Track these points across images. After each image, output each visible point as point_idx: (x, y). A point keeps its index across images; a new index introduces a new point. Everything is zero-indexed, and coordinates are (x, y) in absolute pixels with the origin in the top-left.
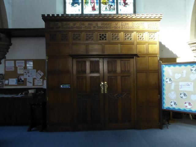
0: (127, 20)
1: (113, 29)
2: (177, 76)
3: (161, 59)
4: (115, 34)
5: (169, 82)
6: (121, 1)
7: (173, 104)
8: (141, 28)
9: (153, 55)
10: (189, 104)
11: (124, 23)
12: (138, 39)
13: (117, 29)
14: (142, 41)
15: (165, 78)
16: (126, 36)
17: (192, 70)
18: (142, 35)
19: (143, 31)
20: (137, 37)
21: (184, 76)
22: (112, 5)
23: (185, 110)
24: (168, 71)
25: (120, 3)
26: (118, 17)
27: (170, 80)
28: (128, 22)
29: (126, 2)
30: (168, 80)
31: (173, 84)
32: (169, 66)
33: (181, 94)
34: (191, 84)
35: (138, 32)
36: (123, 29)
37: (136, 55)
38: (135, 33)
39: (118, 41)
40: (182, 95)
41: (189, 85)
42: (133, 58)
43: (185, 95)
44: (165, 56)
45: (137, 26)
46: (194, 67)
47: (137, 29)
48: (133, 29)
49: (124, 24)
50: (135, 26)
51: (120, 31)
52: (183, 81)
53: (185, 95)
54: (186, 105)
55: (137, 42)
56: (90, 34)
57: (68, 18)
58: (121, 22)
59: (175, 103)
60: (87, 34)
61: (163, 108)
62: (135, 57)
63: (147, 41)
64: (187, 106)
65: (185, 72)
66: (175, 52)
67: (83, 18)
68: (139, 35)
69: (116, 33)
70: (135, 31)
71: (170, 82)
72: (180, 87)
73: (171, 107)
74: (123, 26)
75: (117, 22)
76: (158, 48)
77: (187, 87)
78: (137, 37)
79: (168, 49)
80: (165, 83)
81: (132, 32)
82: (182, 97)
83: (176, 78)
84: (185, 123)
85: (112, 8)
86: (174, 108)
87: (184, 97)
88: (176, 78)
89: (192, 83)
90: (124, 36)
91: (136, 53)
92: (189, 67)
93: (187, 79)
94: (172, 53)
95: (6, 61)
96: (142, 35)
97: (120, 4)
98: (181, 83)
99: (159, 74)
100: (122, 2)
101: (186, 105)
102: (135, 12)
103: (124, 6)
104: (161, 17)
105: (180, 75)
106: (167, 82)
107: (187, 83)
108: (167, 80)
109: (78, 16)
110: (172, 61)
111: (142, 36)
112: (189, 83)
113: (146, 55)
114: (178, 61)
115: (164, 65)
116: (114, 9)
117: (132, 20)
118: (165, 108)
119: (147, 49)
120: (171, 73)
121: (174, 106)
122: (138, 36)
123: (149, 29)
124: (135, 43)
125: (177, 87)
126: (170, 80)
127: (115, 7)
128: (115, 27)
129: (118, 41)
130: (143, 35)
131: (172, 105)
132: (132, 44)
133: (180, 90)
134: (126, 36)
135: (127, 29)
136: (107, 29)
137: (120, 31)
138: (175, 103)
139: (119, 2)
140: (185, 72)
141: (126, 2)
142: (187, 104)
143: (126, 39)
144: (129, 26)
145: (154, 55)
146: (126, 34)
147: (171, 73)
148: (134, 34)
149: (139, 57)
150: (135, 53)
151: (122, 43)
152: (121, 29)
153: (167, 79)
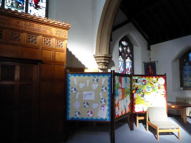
0: (42, 23)
1: (14, 27)
2: (82, 85)
3: (67, 68)
4: (14, 34)
5: (74, 92)
6: (32, 1)
7: (77, 113)
8: (48, 33)
9: (59, 63)
10: (91, 112)
11: (28, 23)
12: (44, 44)
13: (18, 28)
14: (49, 47)
15: (70, 88)
16: (29, 38)
17: (94, 80)
18: (61, 43)
19: (51, 37)
20: (56, 43)
21: (88, 86)
22: (20, 3)
23: (87, 119)
24: (74, 80)
25: (31, 3)
26: (27, 16)
27: (75, 89)
28: (33, 24)
29: (38, 5)
30: (73, 89)
31: (78, 93)
32: (79, 76)
33: (84, 103)
34: (93, 93)
35: (44, 36)
36: (27, 30)
37: (41, 62)
38: (41, 37)
39: (18, 43)
40: (86, 104)
41: (91, 94)
42: (37, 64)
43: (88, 104)
44: (74, 66)
45: (43, 30)
46: (95, 77)
47: (43, 33)
48: (39, 32)
49: (28, 24)
50: (41, 29)
51: (23, 31)
52: (86, 91)
53: (88, 104)
54: (88, 114)
55: (43, 48)
56: (16, 34)
57: (17, 14)
58: (38, 25)
59: (79, 113)
60: (12, 33)
61: (67, 119)
62: (39, 63)
63: (54, 47)
64: (89, 115)
65: (88, 81)
66: (83, 63)
67: (30, 18)
68: (58, 42)
69: (17, 33)
70: (41, 35)
71: (75, 92)
72: (84, 96)
73: (75, 117)
74: (27, 27)
75: (20, 21)
76: (66, 56)
77: (90, 96)
78: (56, 43)
79: (77, 60)
80: (70, 92)
81: (38, 35)
82: (85, 106)
83: (81, 87)
84: (177, 122)
85: (20, 6)
86: (78, 118)
87: (87, 106)
88: (81, 87)
89: (94, 92)
90: (28, 38)
91: (41, 59)
92: (92, 77)
93: (90, 89)
94: (80, 63)
95: (135, 74)
96: (61, 43)
97: (31, 5)
98: (84, 93)
99: (65, 83)
100: (33, 3)
101: (88, 114)
102: (47, 16)
103: (36, 8)
104: (69, 27)
105: (84, 84)
106: (72, 91)
107: (89, 92)
108: (72, 90)
109: (4, 9)
110: (80, 70)
111: (61, 43)
112: (92, 93)
113: (52, 62)
114: (86, 71)
115: (110, 76)
116: (23, 7)
117: (42, 23)
118: (70, 119)
119: (54, 56)
120: (76, 83)
121: (78, 116)
122: (57, 43)
123: (57, 36)
124: (41, 47)
125: (81, 96)
126: (75, 89)
127: (25, 6)
128: (16, 25)
129: (18, 42)
130: (63, 43)
131: (76, 115)
132: (37, 48)
133: (84, 99)
134: (29, 38)
135: (32, 31)
136: (4, 26)
137: (23, 31)
138: (79, 113)
139: (30, 1)
140: (88, 81)
141: (38, 5)
142: (89, 113)
143: (29, 42)
144: (34, 28)
145: (61, 63)
146: (57, 41)
147: (76, 83)
148: (53, 40)
149: (44, 64)
150: (40, 59)
151: (23, 46)
152: (23, 29)
153: (72, 88)
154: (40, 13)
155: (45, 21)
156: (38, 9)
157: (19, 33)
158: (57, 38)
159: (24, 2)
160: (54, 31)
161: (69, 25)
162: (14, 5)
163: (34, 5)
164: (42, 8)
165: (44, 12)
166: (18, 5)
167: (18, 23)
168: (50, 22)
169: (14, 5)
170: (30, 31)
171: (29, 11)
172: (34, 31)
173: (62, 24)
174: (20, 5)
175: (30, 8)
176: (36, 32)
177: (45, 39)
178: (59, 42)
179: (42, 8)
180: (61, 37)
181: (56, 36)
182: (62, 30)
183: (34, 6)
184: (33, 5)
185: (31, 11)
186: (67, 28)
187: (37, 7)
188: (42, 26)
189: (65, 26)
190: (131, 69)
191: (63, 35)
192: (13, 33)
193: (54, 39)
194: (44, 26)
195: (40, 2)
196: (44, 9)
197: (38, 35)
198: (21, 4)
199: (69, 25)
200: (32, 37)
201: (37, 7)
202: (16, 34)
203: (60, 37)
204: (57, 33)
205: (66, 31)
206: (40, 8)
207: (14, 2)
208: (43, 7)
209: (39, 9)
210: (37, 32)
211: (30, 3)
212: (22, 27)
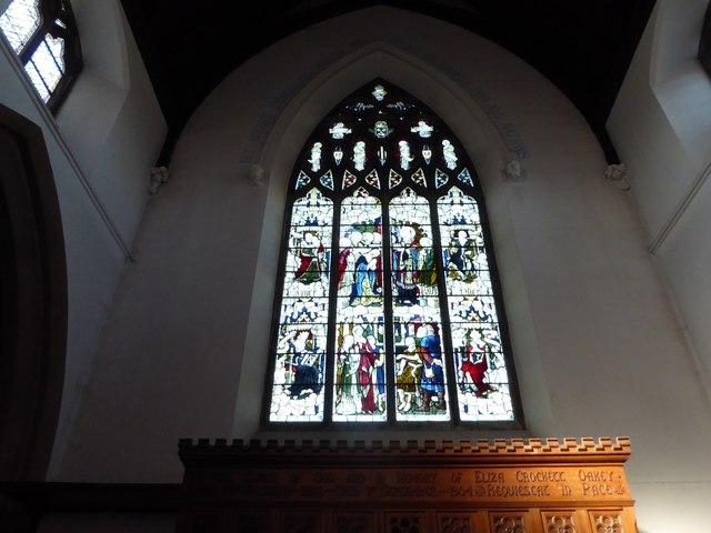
8: (556, 492)
11: (485, 473)
19: (568, 506)
22: (433, 393)
25: (463, 384)
29: (485, 381)
35: (547, 507)
38: (535, 511)
45: (537, 484)
50: (530, 485)
51: (477, 506)
81: (525, 507)
97: (463, 389)
100: (470, 380)
104: (625, 450)
111: (611, 525)
116: (445, 402)
123: (590, 497)
127: (447, 398)
130: (620, 520)
134: (498, 527)
141: (485, 381)
154: (497, 407)
155: (536, 452)
156: (486, 397)
157: (465, 515)
158: (591, 506)
159: (443, 385)
160: (573, 481)
161: (623, 442)
162: (419, 403)
163: (473, 386)
164: (496, 386)
165: (508, 400)
166: (430, 400)
167: (458, 480)
168: (554, 451)
169: (419, 403)
170: (497, 499)
171: (461, 408)
172: (509, 499)
173: (597, 446)
174: (435, 399)
175: (464, 398)
176: (515, 499)
177: (549, 518)
178: (604, 518)
179: (496, 386)
180: (608, 497)
181: (587, 498)
182: (599, 469)
183: (472, 391)
184: (470, 387)
185: (466, 408)
186: (618, 459)
187: (483, 389)
188: (528, 471)
189: (607, 451)
190: (378, 264)
191: (613, 490)
192: (447, 519)
193: (583, 512)
194: (536, 471)
195: (489, 370)
196: (505, 390)
197: (525, 507)
198: (436, 394)
199: (623, 442)
200: (506, 519)
201: (483, 389)
202: (456, 519)
203: (601, 502)
204: (586, 487)
205: (618, 470)
206: (492, 391)
207: (417, 394)
208: (500, 384)
209: (490, 396)
210: (521, 499)
211: (460, 384)
212: (470, 490)
